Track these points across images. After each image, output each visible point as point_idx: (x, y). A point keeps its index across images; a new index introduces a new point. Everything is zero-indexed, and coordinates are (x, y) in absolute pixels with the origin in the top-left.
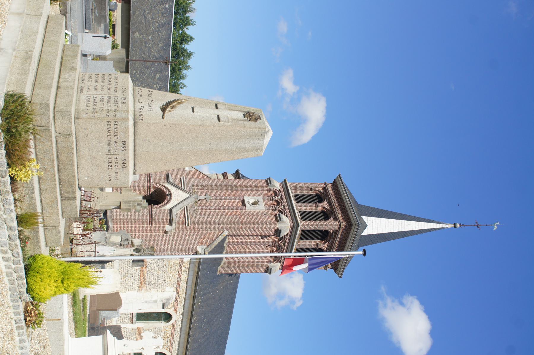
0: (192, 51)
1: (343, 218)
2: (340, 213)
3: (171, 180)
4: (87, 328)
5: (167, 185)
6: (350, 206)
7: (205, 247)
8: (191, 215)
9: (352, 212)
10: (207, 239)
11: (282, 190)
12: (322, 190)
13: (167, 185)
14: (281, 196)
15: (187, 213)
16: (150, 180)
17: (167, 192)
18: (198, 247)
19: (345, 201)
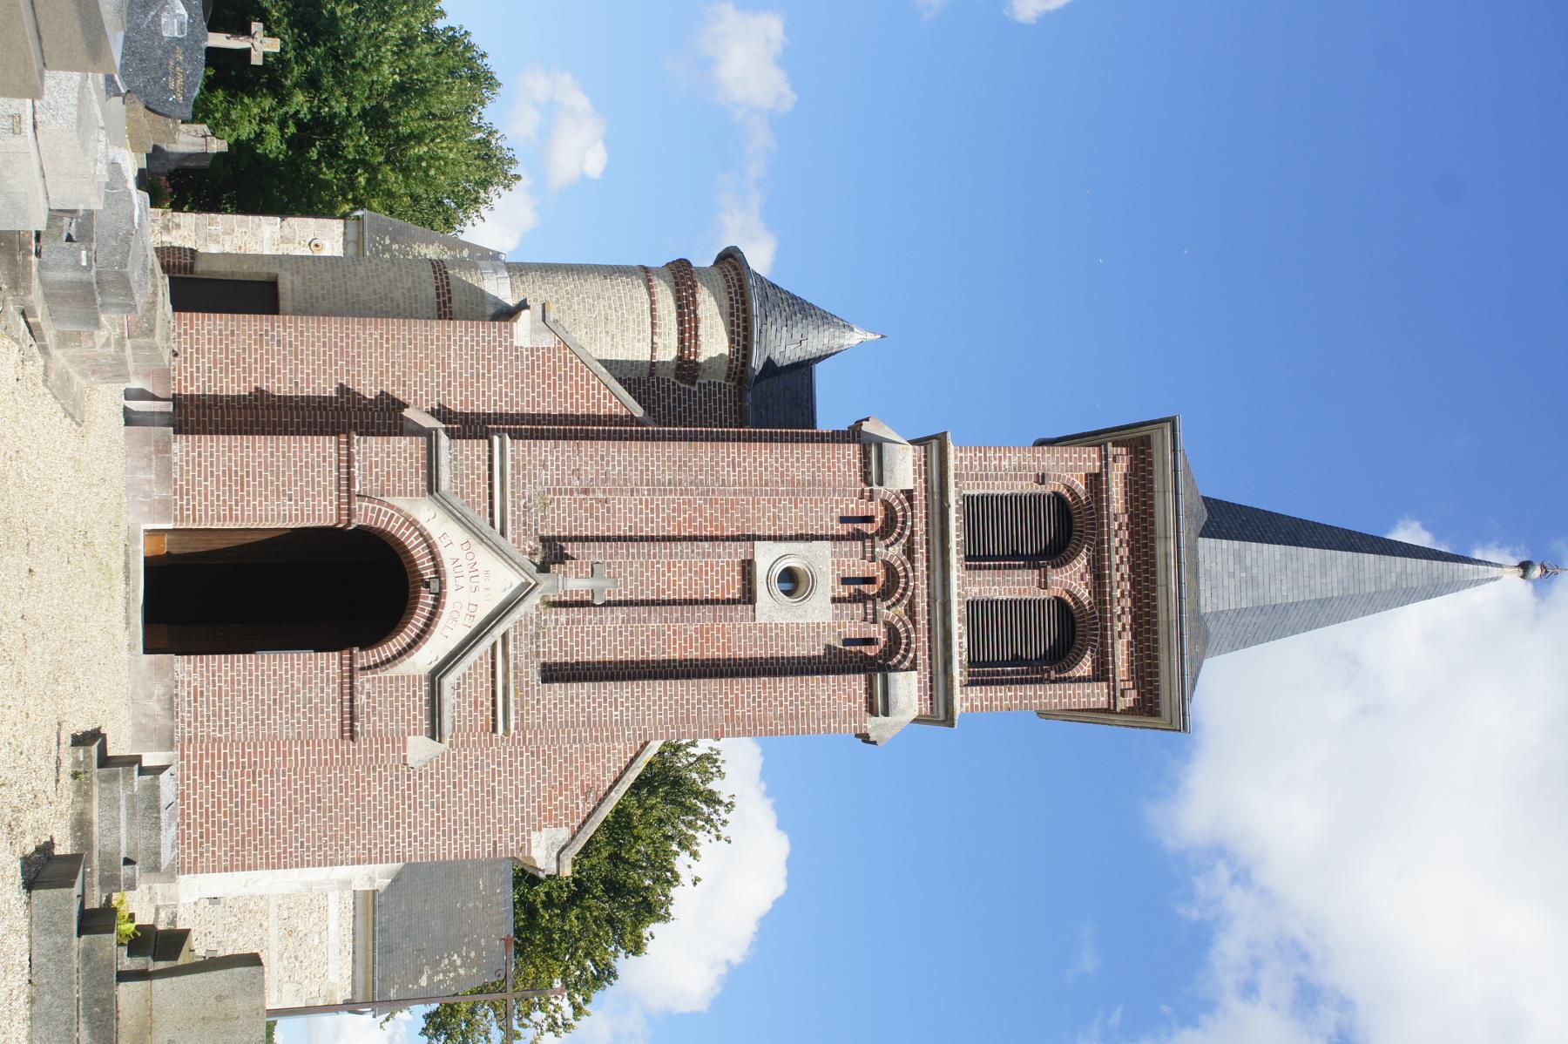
0: (651, 946)
1: (1131, 671)
2: (1127, 636)
3: (445, 484)
4: (34, 270)
5: (427, 514)
6: (1174, 616)
7: (564, 834)
8: (518, 684)
9: (1175, 658)
10: (576, 787)
11: (920, 499)
12: (1080, 487)
13: (427, 514)
14: (911, 541)
15: (506, 676)
16: (350, 479)
17: (428, 574)
18: (535, 836)
19: (1160, 579)
